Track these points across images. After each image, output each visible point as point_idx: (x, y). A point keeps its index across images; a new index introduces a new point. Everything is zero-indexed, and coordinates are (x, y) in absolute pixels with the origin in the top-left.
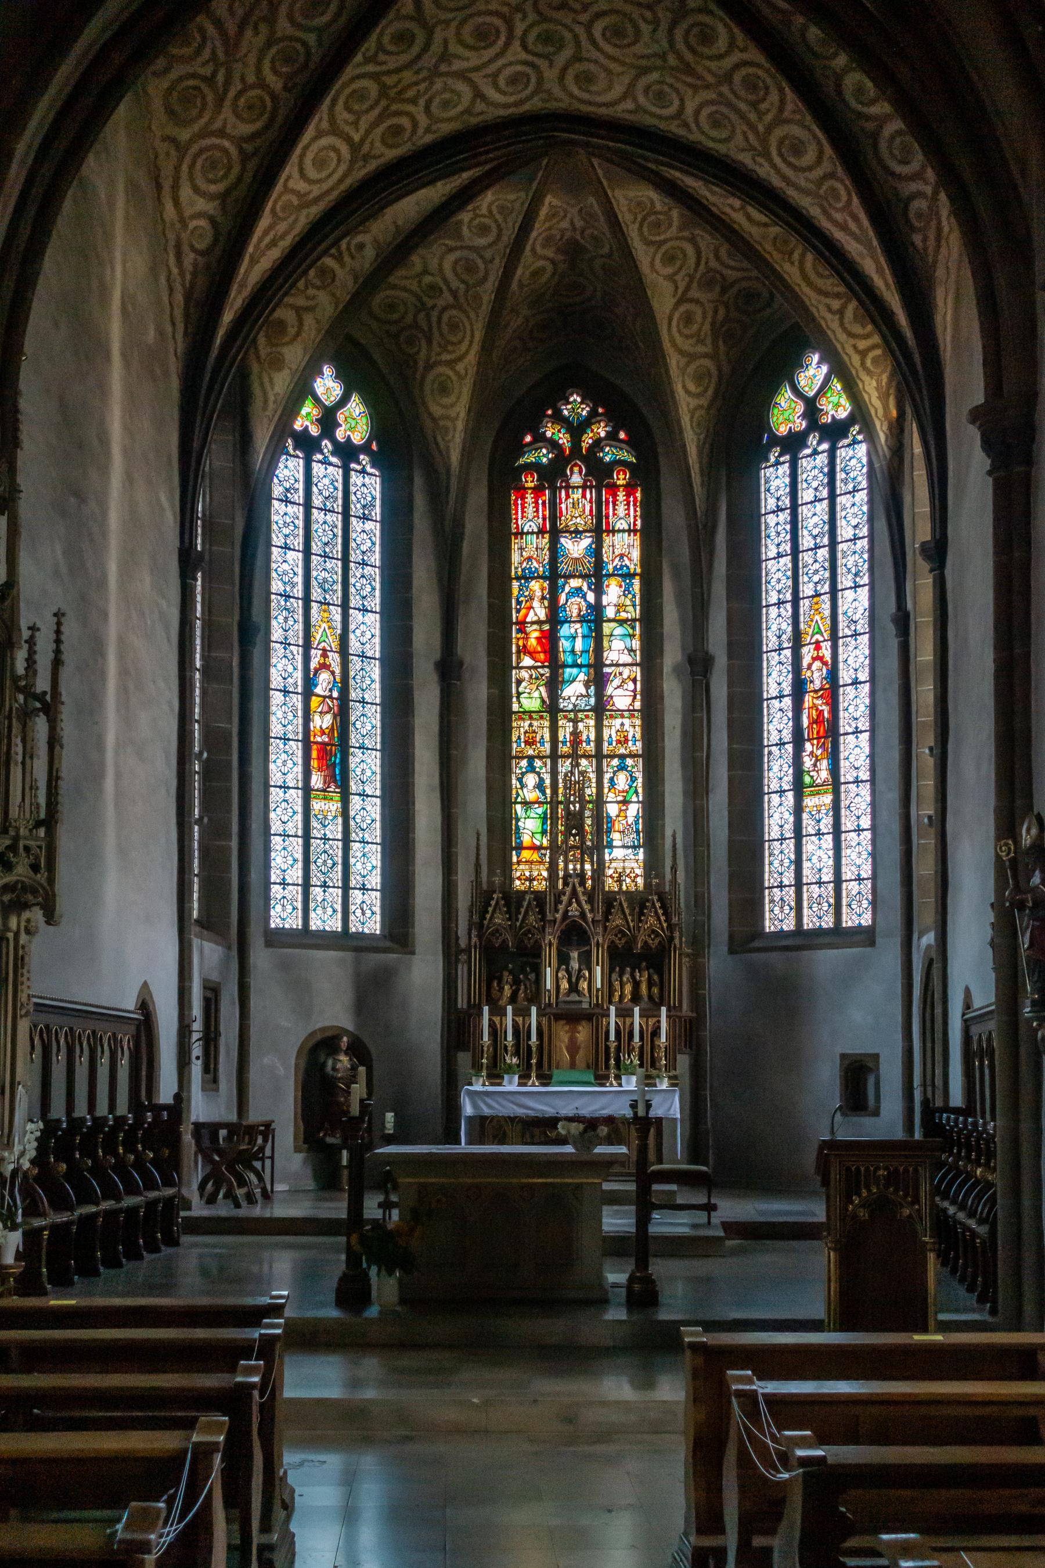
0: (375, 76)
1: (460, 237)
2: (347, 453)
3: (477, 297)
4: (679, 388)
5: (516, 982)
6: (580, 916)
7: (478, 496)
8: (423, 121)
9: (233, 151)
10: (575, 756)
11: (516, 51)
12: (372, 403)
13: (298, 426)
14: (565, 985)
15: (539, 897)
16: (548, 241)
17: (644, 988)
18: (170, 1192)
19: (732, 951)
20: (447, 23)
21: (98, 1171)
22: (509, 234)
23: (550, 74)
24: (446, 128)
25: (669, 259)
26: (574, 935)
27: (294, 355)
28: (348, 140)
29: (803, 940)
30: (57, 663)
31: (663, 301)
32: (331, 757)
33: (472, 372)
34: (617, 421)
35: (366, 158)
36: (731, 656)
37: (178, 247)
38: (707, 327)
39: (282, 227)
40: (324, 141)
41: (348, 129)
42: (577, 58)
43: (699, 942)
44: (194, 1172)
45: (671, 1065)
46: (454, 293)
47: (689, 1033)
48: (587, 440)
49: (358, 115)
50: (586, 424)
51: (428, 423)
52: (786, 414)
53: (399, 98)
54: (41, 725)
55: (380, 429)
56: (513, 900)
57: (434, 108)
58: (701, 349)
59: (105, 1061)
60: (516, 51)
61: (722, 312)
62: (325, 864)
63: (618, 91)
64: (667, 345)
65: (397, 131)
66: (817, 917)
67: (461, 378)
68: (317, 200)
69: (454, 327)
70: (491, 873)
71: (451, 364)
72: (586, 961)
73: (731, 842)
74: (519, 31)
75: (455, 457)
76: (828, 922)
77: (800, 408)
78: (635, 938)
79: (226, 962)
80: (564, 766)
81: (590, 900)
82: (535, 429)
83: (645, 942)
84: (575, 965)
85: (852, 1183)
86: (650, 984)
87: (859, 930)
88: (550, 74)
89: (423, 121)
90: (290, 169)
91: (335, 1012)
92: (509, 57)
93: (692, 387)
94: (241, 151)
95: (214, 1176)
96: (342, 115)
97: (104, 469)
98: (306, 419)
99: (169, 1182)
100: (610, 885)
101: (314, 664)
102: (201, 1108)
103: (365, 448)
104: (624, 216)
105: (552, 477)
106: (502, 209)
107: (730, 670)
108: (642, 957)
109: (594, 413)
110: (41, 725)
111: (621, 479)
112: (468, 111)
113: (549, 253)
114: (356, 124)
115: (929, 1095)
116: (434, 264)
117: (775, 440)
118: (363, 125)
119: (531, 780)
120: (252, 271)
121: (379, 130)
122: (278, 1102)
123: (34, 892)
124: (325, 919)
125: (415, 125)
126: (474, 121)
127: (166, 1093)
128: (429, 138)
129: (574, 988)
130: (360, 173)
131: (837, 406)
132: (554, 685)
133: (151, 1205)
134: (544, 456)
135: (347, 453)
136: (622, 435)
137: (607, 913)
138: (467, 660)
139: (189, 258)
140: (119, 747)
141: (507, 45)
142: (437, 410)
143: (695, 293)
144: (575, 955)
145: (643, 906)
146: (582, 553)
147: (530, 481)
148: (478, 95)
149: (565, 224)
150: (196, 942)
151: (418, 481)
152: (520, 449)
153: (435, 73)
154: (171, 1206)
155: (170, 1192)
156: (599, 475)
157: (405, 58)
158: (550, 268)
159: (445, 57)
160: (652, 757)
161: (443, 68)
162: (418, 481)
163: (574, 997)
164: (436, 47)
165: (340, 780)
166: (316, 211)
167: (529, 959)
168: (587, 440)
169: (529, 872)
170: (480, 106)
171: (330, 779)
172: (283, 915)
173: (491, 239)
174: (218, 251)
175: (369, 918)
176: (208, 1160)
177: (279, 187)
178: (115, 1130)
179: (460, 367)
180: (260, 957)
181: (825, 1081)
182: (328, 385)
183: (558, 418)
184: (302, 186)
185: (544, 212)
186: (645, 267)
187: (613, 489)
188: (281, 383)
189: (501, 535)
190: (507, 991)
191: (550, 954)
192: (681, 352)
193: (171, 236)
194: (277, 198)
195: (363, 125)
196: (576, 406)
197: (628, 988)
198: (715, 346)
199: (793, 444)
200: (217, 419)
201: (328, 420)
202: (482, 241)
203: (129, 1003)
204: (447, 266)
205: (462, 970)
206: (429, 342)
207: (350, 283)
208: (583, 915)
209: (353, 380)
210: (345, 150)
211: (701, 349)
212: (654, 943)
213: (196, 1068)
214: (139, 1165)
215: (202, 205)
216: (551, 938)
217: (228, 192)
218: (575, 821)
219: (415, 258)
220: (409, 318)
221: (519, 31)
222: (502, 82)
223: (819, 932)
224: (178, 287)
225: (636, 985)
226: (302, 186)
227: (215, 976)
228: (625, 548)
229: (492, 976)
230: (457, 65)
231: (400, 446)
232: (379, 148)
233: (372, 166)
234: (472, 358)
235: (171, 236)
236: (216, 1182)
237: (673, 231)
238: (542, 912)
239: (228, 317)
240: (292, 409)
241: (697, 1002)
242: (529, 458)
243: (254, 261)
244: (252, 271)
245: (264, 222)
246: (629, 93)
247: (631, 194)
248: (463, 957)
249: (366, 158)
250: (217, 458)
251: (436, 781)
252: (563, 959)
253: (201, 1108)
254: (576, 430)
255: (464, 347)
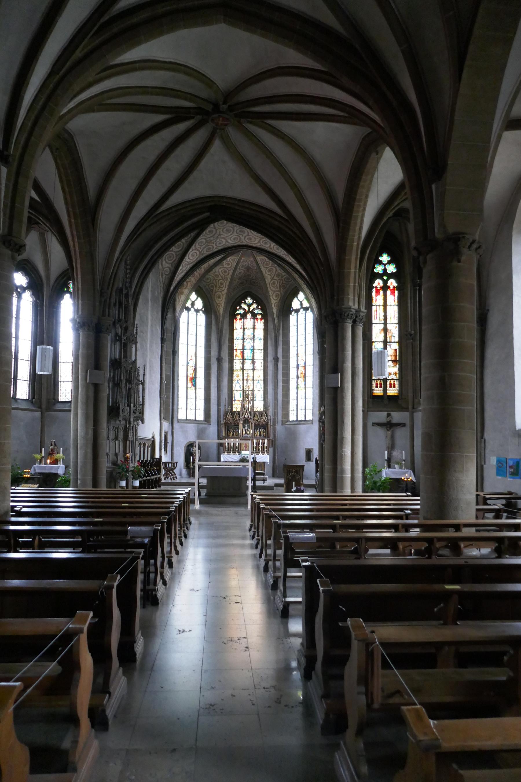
0: (205, 239)
1: (223, 265)
2: (197, 311)
3: (227, 278)
4: (272, 298)
5: (234, 431)
6: (248, 417)
7: (227, 320)
8: (215, 247)
9: (174, 254)
10: (247, 380)
11: (235, 234)
12: (202, 299)
13: (187, 306)
14: (244, 432)
15: (239, 412)
16: (243, 266)
17: (262, 433)
18: (159, 476)
19: (282, 425)
20: (220, 229)
21: (150, 471)
22: (234, 265)
23: (243, 238)
24: (220, 248)
25: (269, 271)
26: (246, 421)
27: (186, 291)
28: (198, 250)
29: (298, 422)
30: (144, 375)
31: (268, 280)
32: (194, 380)
33: (225, 294)
34: (258, 304)
35: (202, 254)
36: (283, 358)
37: (162, 273)
38: (278, 285)
39: (184, 269)
40: (194, 251)
41: (199, 249)
42: (248, 235)
43: (275, 423)
44: (163, 472)
45: (268, 450)
46: (222, 277)
47: (272, 443)
48: (251, 308)
49: (201, 246)
50: (251, 305)
51: (216, 305)
52: (295, 304)
53: (209, 243)
54: (141, 386)
55: (205, 306)
56: (233, 413)
57: (218, 244)
58: (277, 290)
59: (146, 449)
60: (235, 234)
61: (281, 281)
62: (191, 403)
63: (257, 242)
64: (269, 288)
65: (210, 248)
66: (301, 417)
67: (223, 295)
68: (191, 263)
69: (222, 284)
70: (228, 407)
71: (221, 292)
72: (249, 427)
73: (282, 400)
74: (235, 230)
75: (221, 312)
76: (303, 419)
77: (299, 303)
78: (260, 422)
79: (169, 426)
80: (245, 382)
81: (250, 414)
82: (240, 305)
83: (262, 424)
84: (246, 428)
85: (288, 472)
86: (263, 432)
87: (310, 420)
88: (243, 238)
89: (215, 247)
90: (186, 257)
91: (192, 437)
92: (233, 234)
93: (275, 298)
94: (176, 254)
95: (166, 474)
96: (197, 246)
97: (147, 326)
98: (189, 304)
99: (159, 474)
100: (255, 410)
101: (189, 359)
102: (164, 459)
103: (201, 310)
104: (260, 262)
105: (243, 316)
106: (232, 260)
107: (283, 361)
108: (262, 426)
109: (253, 302)
110: (141, 386)
111: (259, 317)
112: (225, 244)
113: (243, 269)
114: (200, 248)
115: (117, 451)
116: (217, 270)
117: (293, 310)
118: (202, 248)
119: (238, 385)
120: (178, 278)
121: (205, 249)
122: (180, 458)
123: (139, 418)
124: (191, 417)
125: (213, 247)
126: (226, 246)
127: (157, 456)
128: (216, 250)
129: (246, 433)
130: (201, 257)
131: (306, 304)
132: (243, 363)
133: (156, 478)
134: (242, 312)
135: (197, 311)
136: (259, 307)
137: (254, 416)
138: (224, 358)
139: (164, 276)
140: (149, 382)
141: (233, 233)
142: (218, 302)
143: (275, 277)
144: (246, 426)
145: (262, 415)
146: (249, 332)
147: (238, 317)
148: (227, 241)
149: (246, 263)
150: (163, 422)
151: (213, 316)
152: (237, 310)
153: (218, 238)
154: (159, 479)
155: (159, 476)
156: (254, 316)
157: (211, 235)
158: (243, 271)
159: (220, 235)
160: (265, 381)
161: (219, 237)
162: (213, 316)
163: (246, 435)
164: (218, 233)
165: (195, 385)
166: (191, 265)
167: (237, 426)
168: (251, 308)
169: (237, 407)
170: (227, 244)
171: (193, 385)
172: (181, 415)
173: (230, 266)
174: (170, 274)
175: (201, 417)
176: (165, 470)
177: (184, 261)
178: (149, 463)
179: (223, 292)
180: (176, 425)
181: (302, 454)
182: (193, 296)
183: (245, 303)
184: (189, 260)
185: (241, 261)
186: (264, 273)
187: (257, 319)
188: (183, 298)
189: (232, 329)
190: (231, 434)
191: (241, 426)
192: (272, 290)
193: (161, 272)
194: (184, 263)
195: (202, 248)
196: (249, 300)
197: (258, 433)
198: (280, 289)
199: (297, 311)
200: (169, 308)
201: (193, 304)
202: (227, 266)
203: (150, 437)
204: (220, 270)
205: (221, 428)
206: (216, 287)
207: (198, 276)
208: (248, 417)
209: (199, 295)
210: (198, 253)
211: (277, 290)
212: (264, 423)
213: (163, 450)
214: (153, 470)
215: (167, 265)
216: (241, 422)
217: (173, 262)
218: (247, 396)
219: (214, 270)
220: (212, 281)
221: (235, 230)
222: (232, 239)
223: (301, 421)
224: (162, 283)
225: (260, 432)
226: (189, 260)
227: (167, 430)
228: (260, 333)
229: (228, 430)
230: (222, 236)
231: (209, 309)
232: (205, 252)
233: (204, 256)
234: (226, 291)
235: (161, 272)
236: (166, 476)
237: (270, 265)
238: (239, 416)
239: (172, 288)
240: (186, 302)
241: (275, 436)
242: (238, 312)
243: (178, 276)
244: (178, 278)
245: (180, 268)
246: (259, 242)
247: (261, 258)
248: (222, 426)
249: (203, 254)
250: (169, 315)
251: (216, 385)
252: (244, 427)
253: (164, 459)
254: (249, 306)
255: (224, 288)
